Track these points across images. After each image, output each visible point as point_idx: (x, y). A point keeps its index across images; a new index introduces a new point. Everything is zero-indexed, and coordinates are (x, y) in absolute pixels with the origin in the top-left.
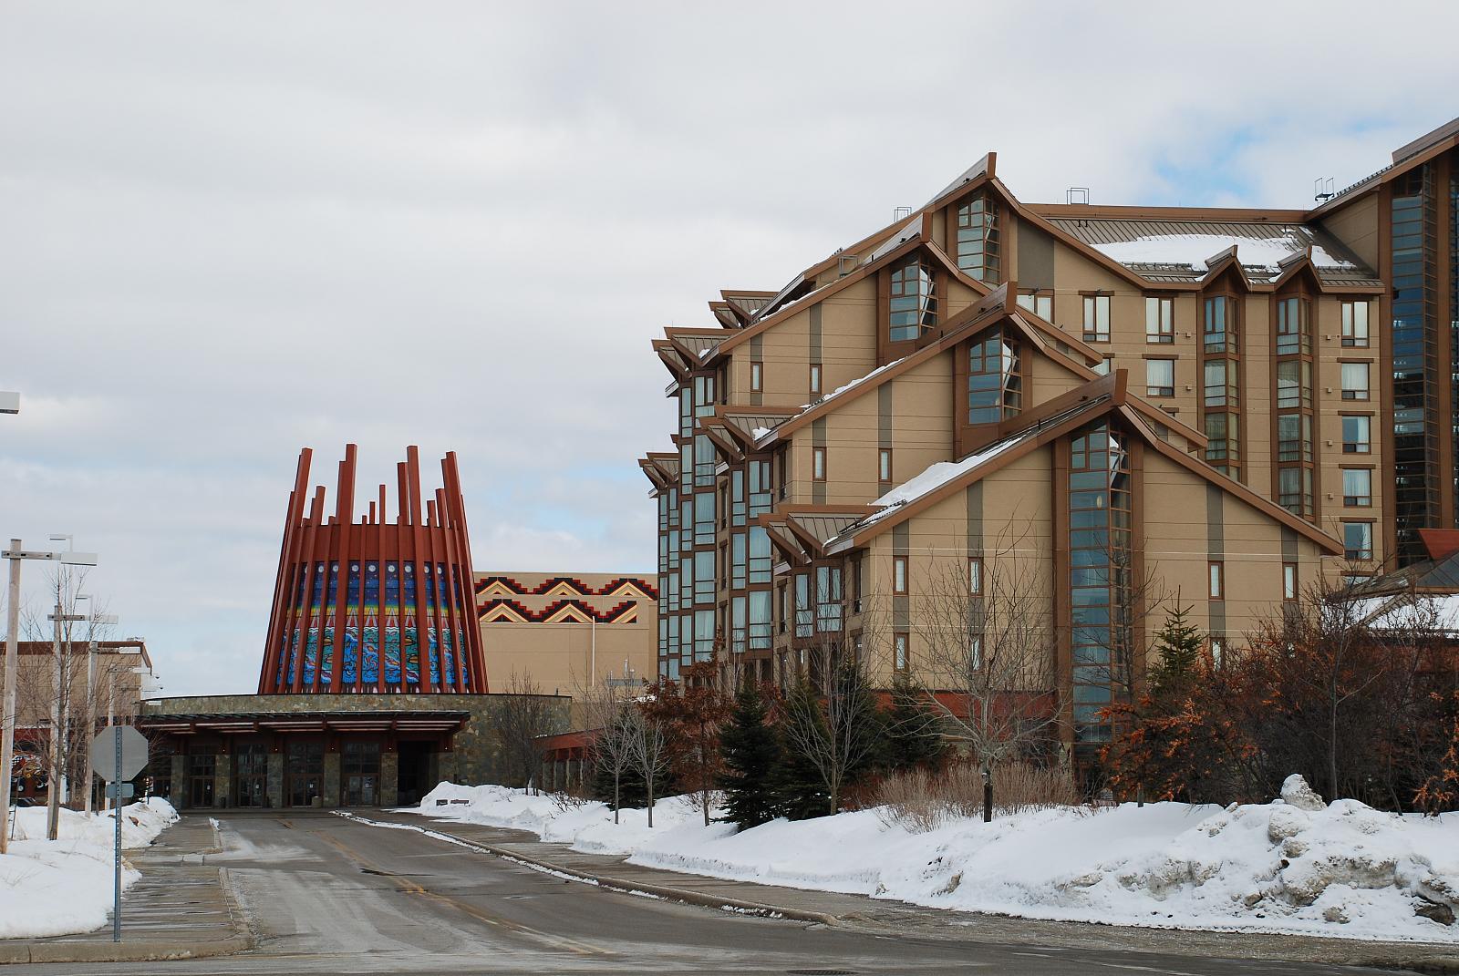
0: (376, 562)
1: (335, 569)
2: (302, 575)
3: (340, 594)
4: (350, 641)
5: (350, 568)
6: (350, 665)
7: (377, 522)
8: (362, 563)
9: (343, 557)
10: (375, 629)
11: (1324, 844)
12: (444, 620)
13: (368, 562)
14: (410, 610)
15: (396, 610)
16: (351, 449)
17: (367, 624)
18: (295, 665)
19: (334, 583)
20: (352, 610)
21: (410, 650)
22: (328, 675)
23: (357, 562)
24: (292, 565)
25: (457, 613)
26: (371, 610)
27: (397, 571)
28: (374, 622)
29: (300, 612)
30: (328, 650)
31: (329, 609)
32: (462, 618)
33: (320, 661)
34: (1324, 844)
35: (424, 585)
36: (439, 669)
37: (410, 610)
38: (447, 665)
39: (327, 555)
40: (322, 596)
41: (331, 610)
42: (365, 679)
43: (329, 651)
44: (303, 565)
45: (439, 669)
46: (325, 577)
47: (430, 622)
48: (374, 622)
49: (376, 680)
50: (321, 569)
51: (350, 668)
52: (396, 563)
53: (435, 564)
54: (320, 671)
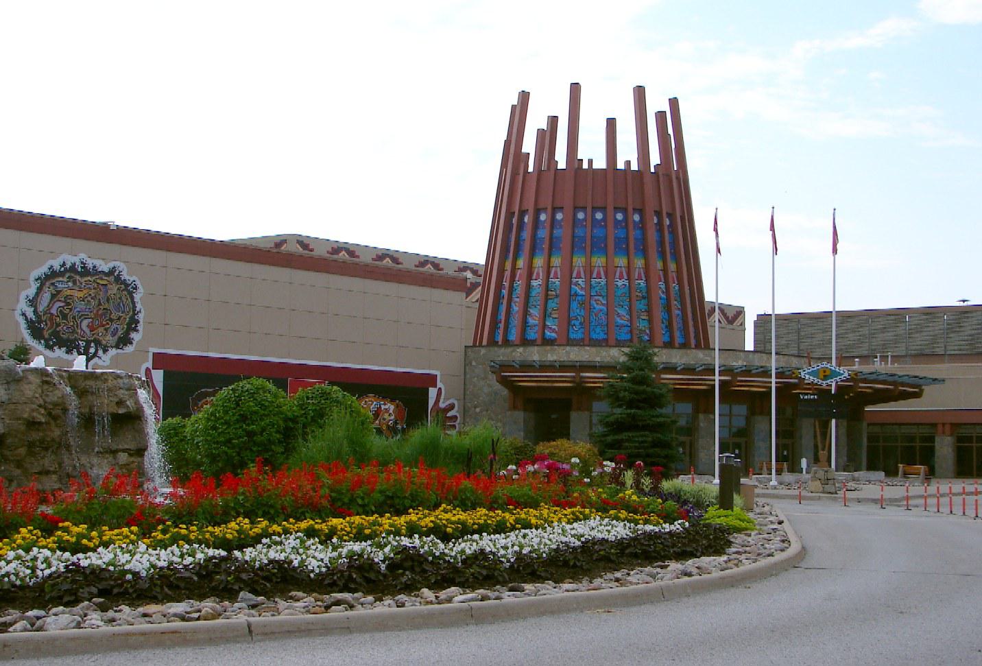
0: (603, 209)
1: (559, 216)
2: (521, 224)
3: (566, 244)
4: (576, 295)
5: (575, 215)
6: (577, 319)
7: (561, 161)
8: (589, 210)
9: (568, 203)
10: (603, 281)
11: (211, 639)
12: (672, 275)
13: (595, 209)
14: (639, 263)
15: (603, 260)
16: (575, 89)
17: (594, 276)
18: (516, 321)
19: (557, 232)
20: (579, 261)
21: (641, 305)
22: (554, 331)
23: (584, 209)
24: (510, 214)
25: (672, 266)
26: (599, 261)
27: (626, 219)
28: (602, 273)
29: (539, 262)
30: (552, 304)
31: (553, 259)
32: (679, 271)
33: (545, 315)
34: (211, 639)
35: (652, 236)
36: (670, 327)
37: (639, 263)
38: (677, 323)
39: (589, 198)
40: (546, 246)
41: (556, 261)
42: (594, 336)
43: (554, 305)
44: (523, 213)
45: (670, 327)
46: (547, 225)
47: (538, 274)
48: (602, 273)
49: (605, 337)
50: (543, 217)
51: (577, 323)
52: (624, 211)
53: (630, 209)
54: (544, 326)
